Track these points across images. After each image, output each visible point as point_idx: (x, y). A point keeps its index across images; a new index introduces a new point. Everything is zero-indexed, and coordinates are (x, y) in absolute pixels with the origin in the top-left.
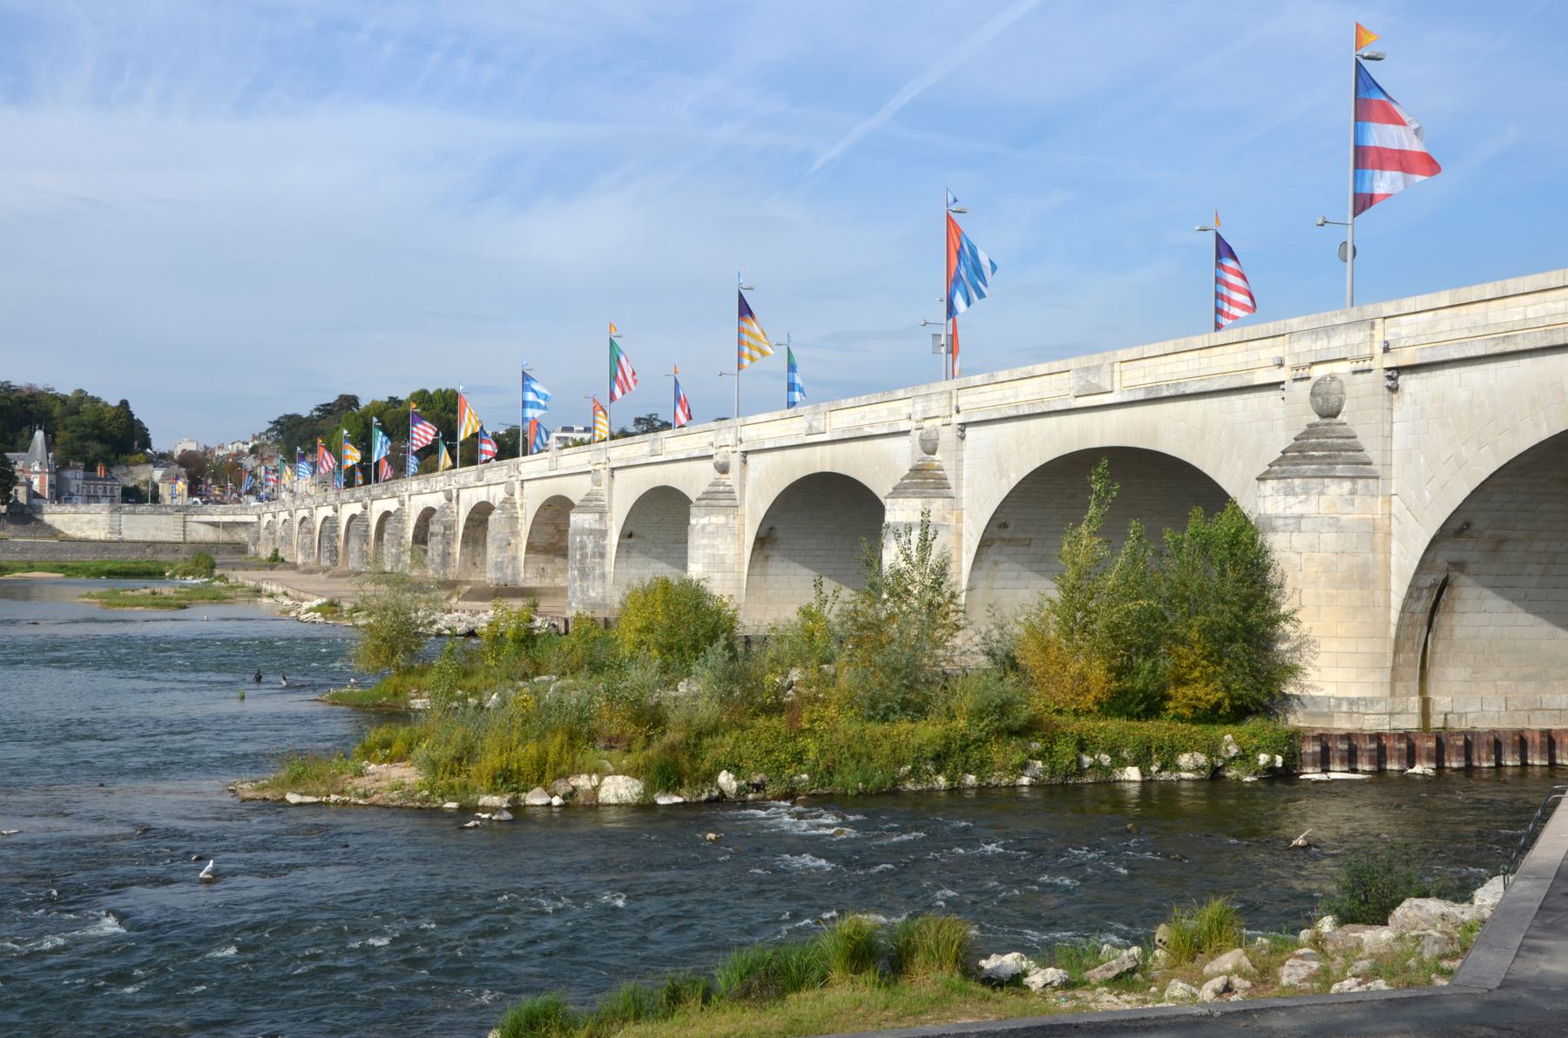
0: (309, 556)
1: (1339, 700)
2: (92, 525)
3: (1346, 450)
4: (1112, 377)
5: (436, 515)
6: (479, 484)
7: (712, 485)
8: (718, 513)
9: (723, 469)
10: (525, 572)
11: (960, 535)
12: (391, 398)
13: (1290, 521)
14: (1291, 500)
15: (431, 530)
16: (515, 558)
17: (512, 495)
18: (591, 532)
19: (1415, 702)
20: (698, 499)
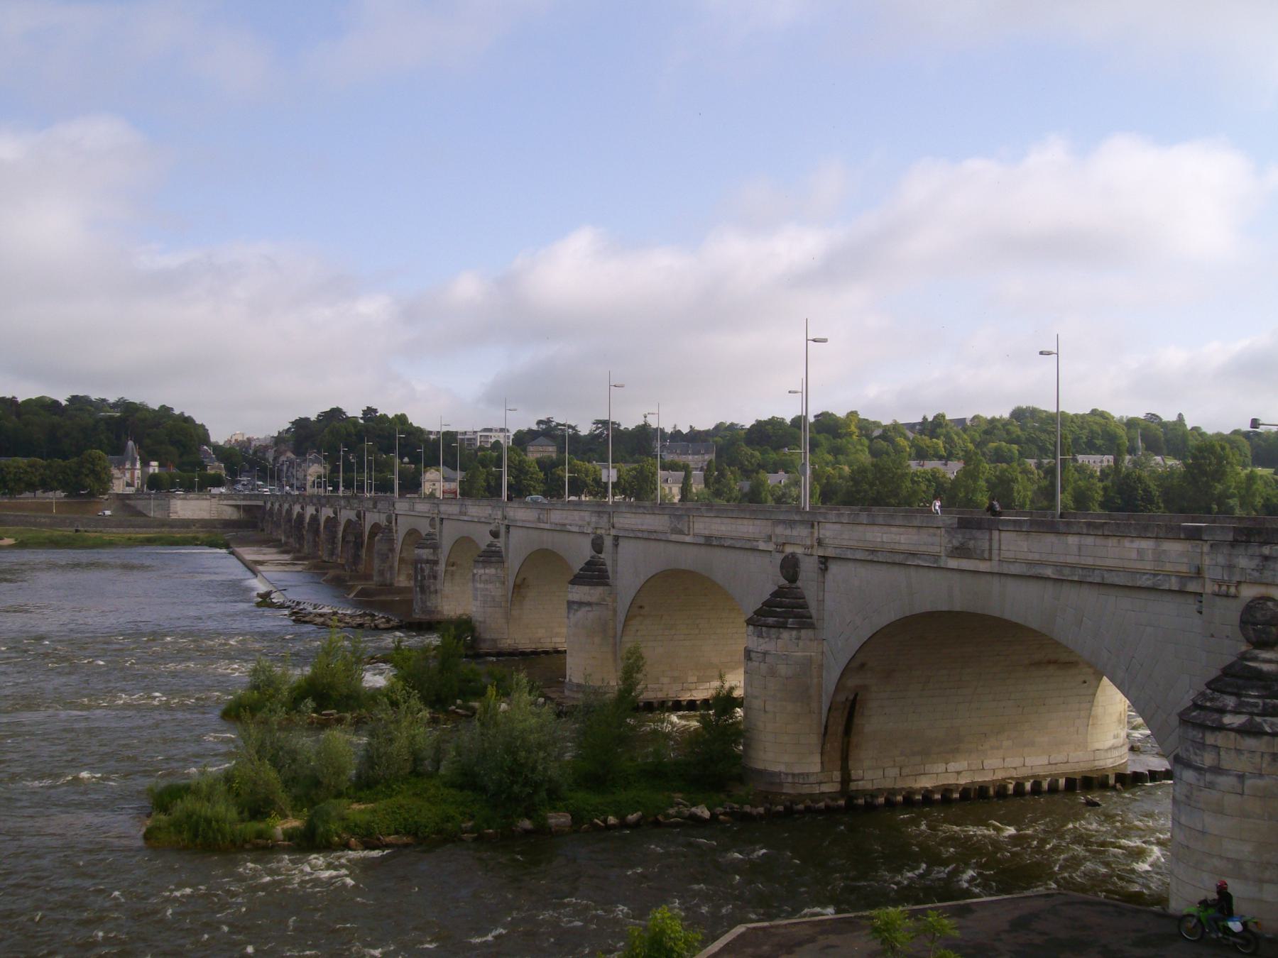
1: (787, 774)
3: (797, 608)
4: (689, 525)
7: (488, 546)
8: (491, 567)
9: (495, 534)
11: (615, 611)
12: (368, 407)
13: (759, 655)
14: (761, 640)
18: (428, 562)
19: (837, 775)
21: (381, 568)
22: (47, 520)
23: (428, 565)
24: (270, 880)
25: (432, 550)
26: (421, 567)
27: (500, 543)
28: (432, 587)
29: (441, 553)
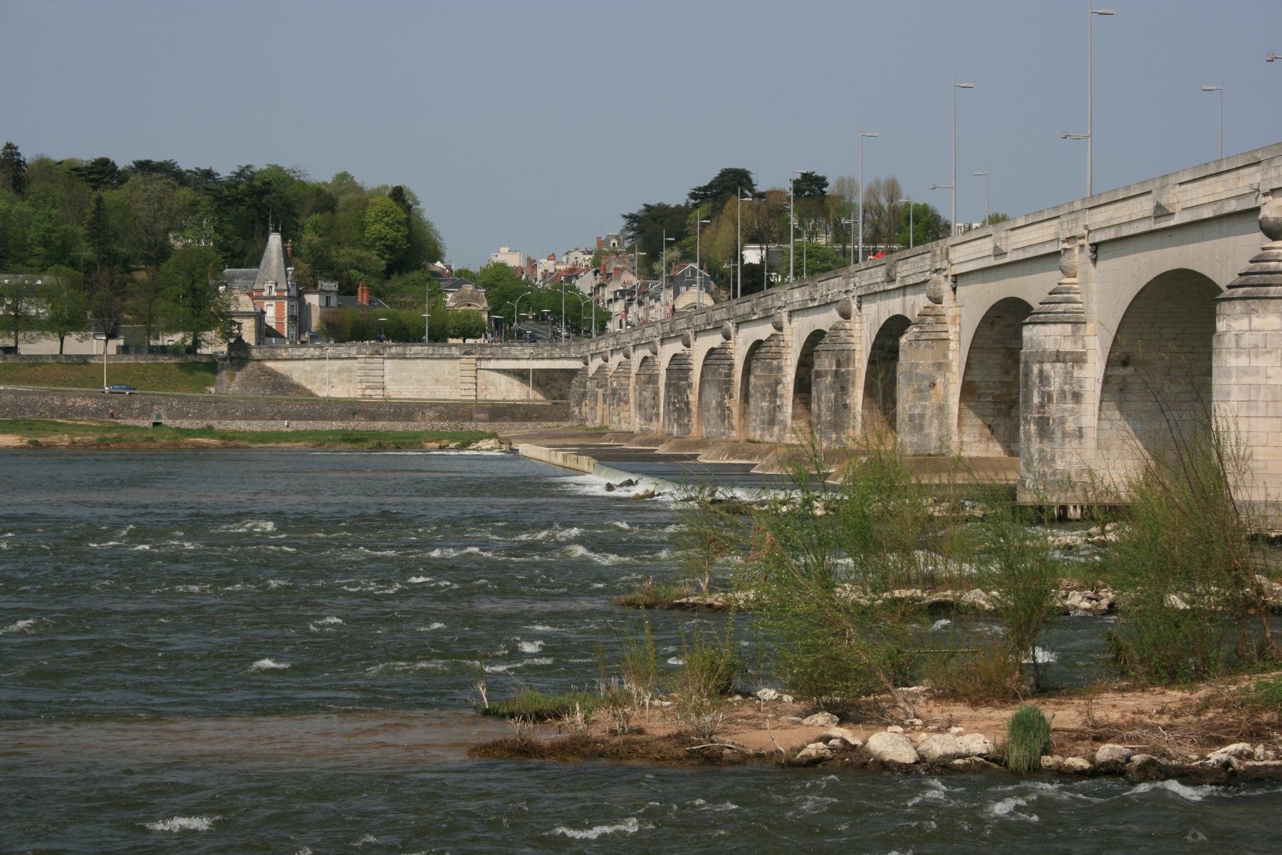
0: (651, 420)
2: (344, 375)
5: (827, 339)
10: (960, 431)
15: (816, 368)
16: (942, 409)
18: (1059, 357)
20: (1229, 287)
21: (917, 411)
22: (91, 403)
23: (1059, 365)
25: (1069, 327)
26: (1041, 371)
28: (1070, 419)
29: (831, 719)
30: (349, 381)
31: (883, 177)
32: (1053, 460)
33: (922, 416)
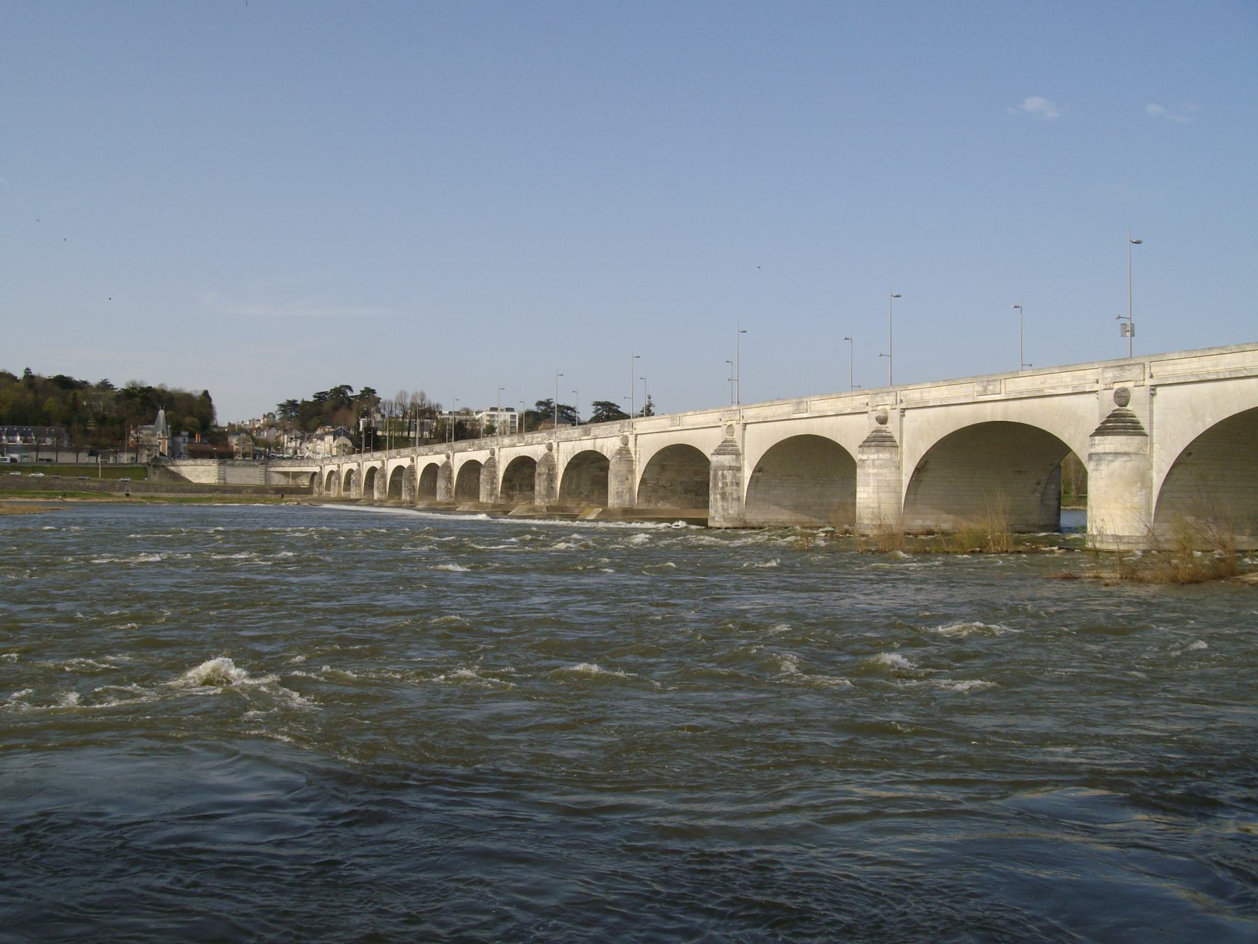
2: (206, 473)
6: (586, 437)
8: (885, 451)
12: (366, 388)
17: (626, 445)
18: (730, 468)
22: (96, 485)
24: (265, 692)
25: (734, 456)
27: (891, 427)
30: (208, 476)
31: (419, 391)
32: (728, 509)
33: (622, 492)
